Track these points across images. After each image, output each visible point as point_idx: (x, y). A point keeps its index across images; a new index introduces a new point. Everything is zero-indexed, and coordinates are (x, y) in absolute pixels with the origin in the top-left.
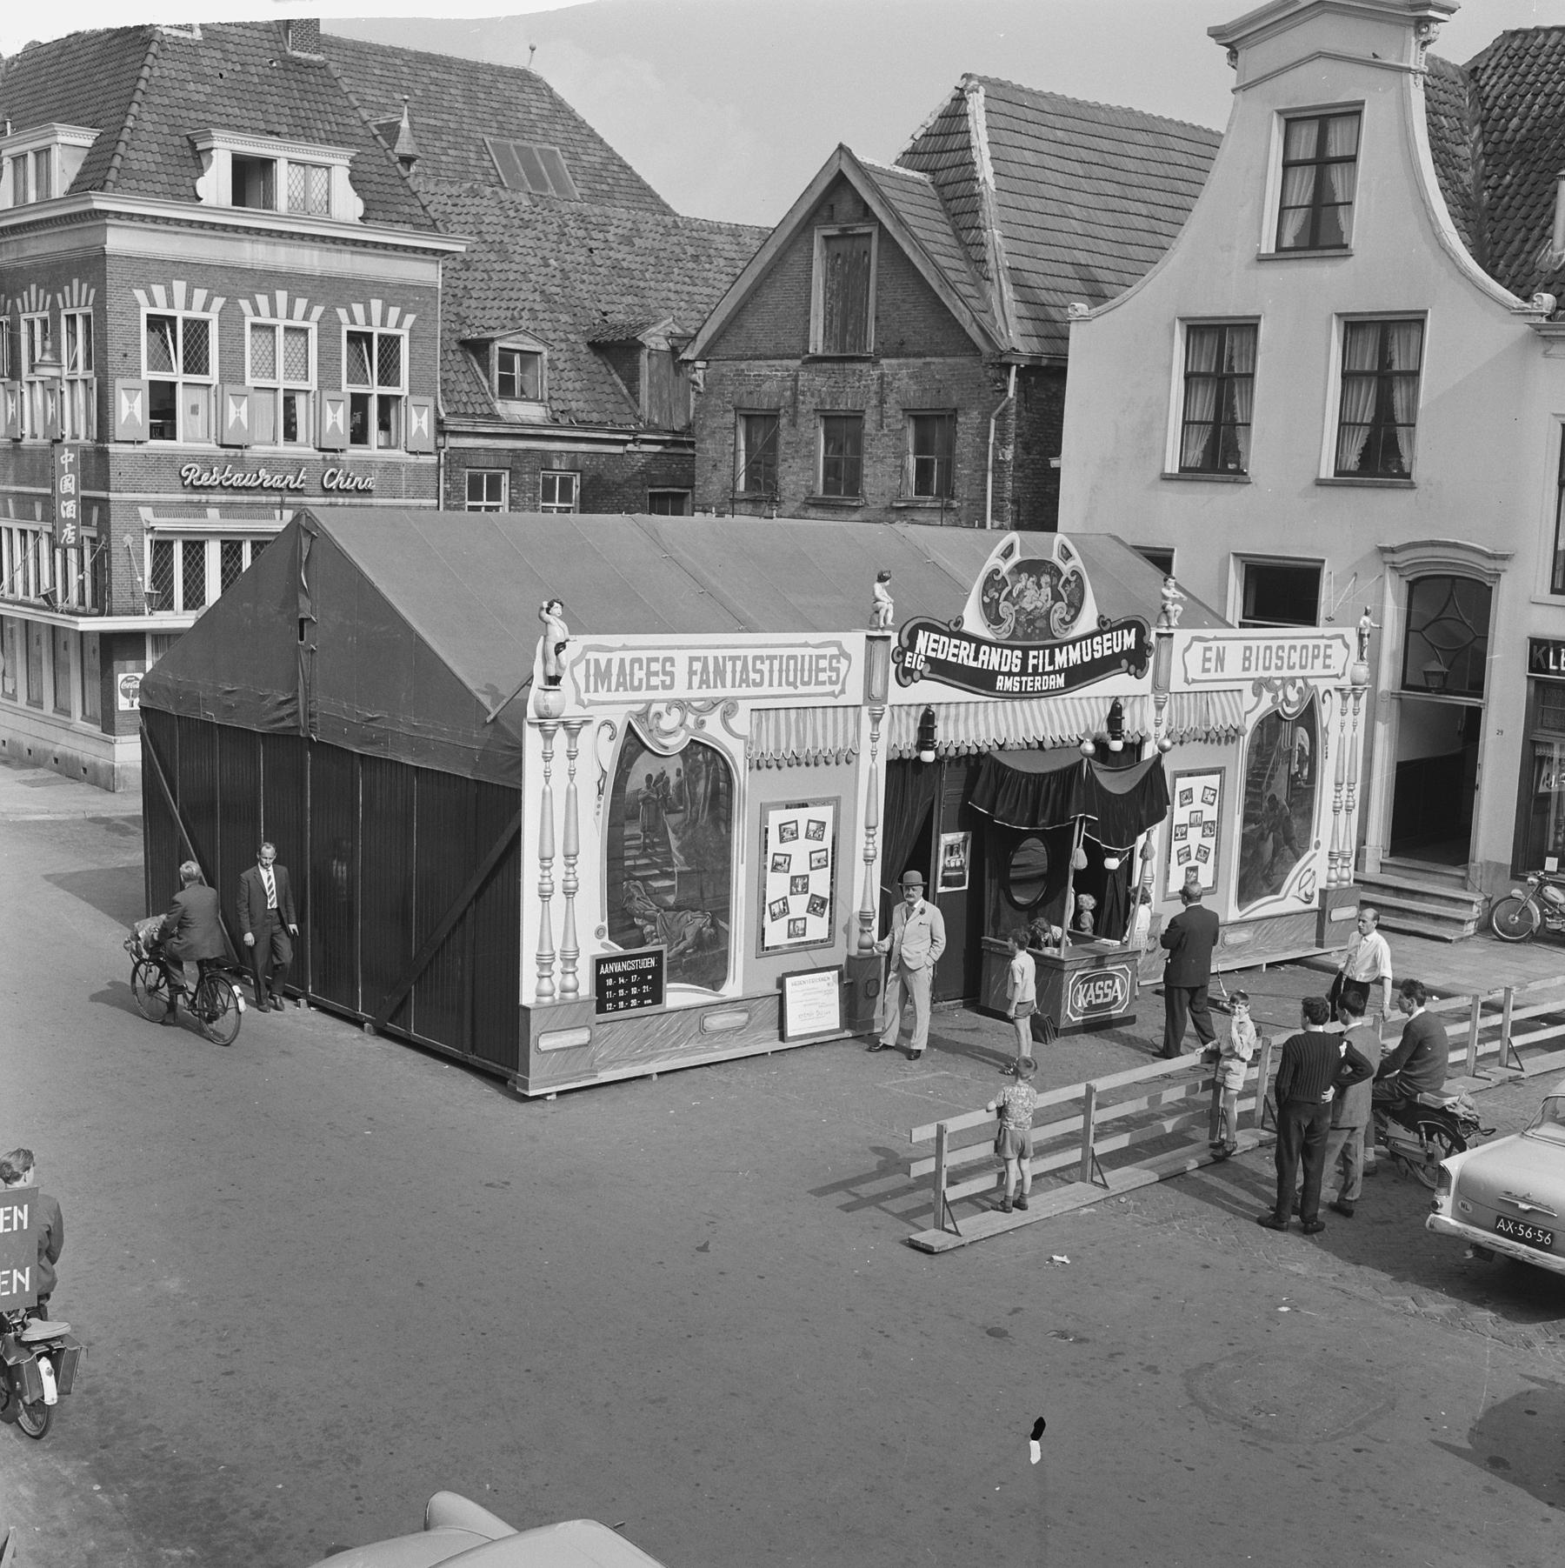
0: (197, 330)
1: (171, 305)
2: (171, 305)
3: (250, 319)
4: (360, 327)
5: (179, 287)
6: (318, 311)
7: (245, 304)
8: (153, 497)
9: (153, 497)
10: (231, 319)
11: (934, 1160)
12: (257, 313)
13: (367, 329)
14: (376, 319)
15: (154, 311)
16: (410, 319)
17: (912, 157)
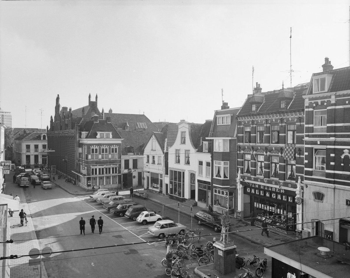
7: (111, 147)
14: (114, 147)
16: (118, 146)
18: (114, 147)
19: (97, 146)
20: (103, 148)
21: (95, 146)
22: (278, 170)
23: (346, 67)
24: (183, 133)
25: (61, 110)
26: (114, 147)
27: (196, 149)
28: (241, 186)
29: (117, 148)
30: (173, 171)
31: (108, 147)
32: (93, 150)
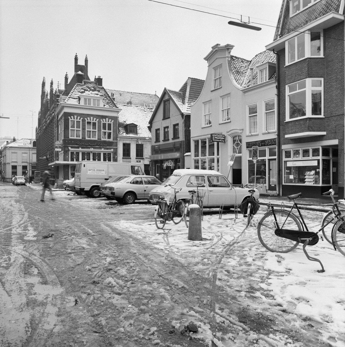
0: (94, 124)
1: (90, 120)
2: (90, 120)
3: (70, 120)
4: (89, 121)
5: (92, 118)
6: (98, 120)
7: (102, 120)
8: (71, 146)
9: (71, 146)
10: (99, 122)
11: (334, 224)
12: (88, 120)
13: (74, 120)
14: (107, 121)
15: (103, 122)
16: (113, 121)
17: (180, 90)
18: (106, 121)
19: (110, 120)
20: (105, 122)
21: (107, 119)
22: (274, 192)
23: (290, 109)
24: (7, 230)
25: (310, 344)
26: (106, 121)
27: (342, 213)
28: (297, 11)
29: (81, 120)
30: (305, 87)
31: (82, 119)
32: (104, 125)
